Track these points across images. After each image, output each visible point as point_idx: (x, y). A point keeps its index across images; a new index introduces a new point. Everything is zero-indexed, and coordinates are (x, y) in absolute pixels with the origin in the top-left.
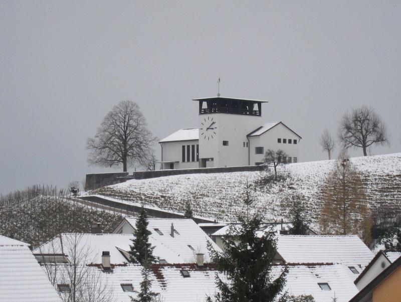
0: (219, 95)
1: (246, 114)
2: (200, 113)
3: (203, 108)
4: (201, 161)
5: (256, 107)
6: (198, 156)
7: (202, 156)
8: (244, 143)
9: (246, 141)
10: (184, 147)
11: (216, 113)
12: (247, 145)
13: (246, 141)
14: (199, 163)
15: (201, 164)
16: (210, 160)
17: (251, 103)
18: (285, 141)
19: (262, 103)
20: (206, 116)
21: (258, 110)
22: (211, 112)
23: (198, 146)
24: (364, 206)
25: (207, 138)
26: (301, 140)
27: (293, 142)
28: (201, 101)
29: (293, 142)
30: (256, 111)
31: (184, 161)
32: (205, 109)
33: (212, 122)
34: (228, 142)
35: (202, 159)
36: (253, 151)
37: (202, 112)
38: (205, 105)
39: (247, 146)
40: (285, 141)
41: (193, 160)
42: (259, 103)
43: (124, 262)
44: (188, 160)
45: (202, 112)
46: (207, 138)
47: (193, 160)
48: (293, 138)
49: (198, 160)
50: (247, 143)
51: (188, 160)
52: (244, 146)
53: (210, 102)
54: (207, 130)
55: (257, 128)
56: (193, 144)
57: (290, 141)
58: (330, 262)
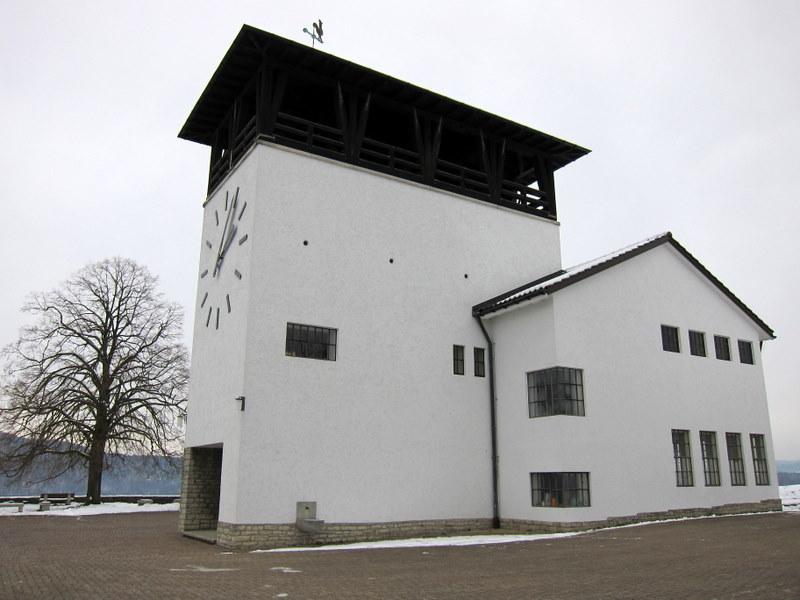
8: (458, 351)
9: (472, 340)
13: (472, 340)
36: (515, 394)
39: (479, 373)
48: (738, 331)
50: (478, 352)
52: (459, 369)
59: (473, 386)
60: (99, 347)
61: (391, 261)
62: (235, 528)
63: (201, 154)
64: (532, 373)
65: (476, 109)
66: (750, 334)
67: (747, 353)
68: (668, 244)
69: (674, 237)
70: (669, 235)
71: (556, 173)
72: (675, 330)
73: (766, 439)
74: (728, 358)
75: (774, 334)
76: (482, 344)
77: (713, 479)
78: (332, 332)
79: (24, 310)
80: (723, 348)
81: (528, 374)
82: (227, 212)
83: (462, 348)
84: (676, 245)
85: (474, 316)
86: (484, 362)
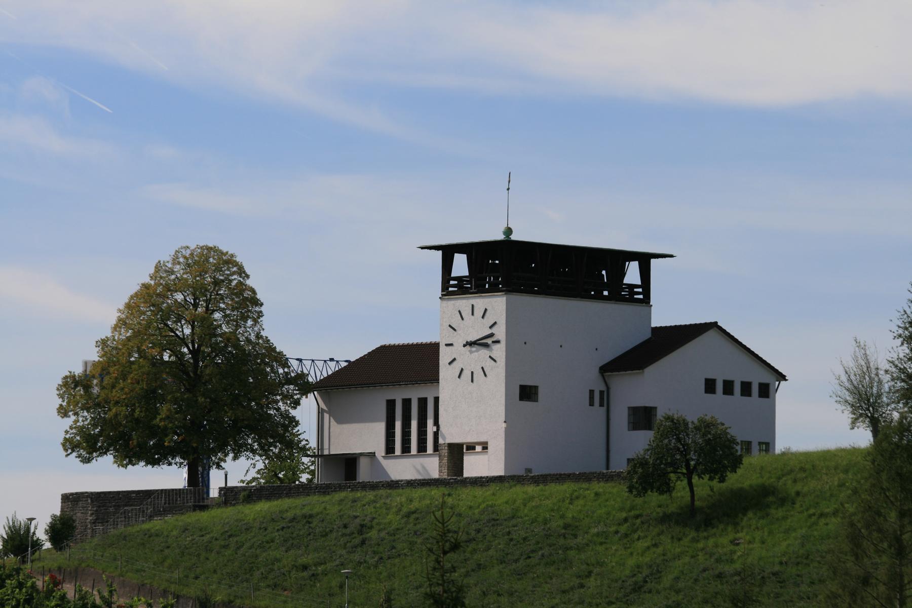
8: (592, 392)
9: (599, 386)
13: (599, 386)
36: (620, 418)
39: (601, 405)
48: (757, 377)
50: (602, 393)
52: (592, 404)
62: (440, 471)
65: (660, 359)
66: (766, 378)
70: (716, 323)
71: (650, 336)
73: (771, 446)
74: (750, 395)
76: (603, 388)
77: (407, 403)
78: (536, 387)
82: (604, 408)
86: (604, 399)
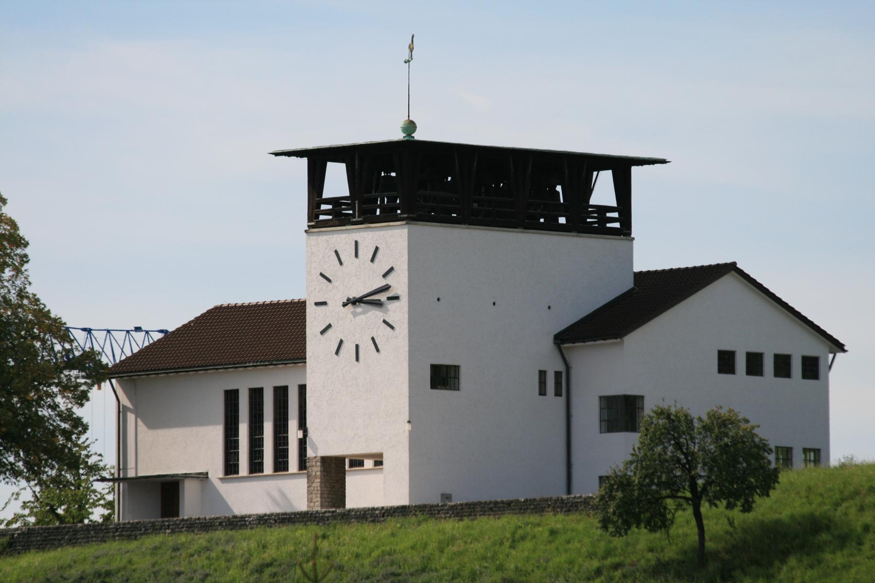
0: (410, 126)
1: (552, 227)
2: (315, 221)
3: (325, 195)
4: (316, 469)
5: (603, 191)
6: (302, 443)
7: (325, 442)
8: (542, 374)
9: (553, 365)
10: (231, 397)
11: (396, 219)
12: (558, 384)
13: (553, 365)
14: (310, 482)
15: (317, 483)
16: (369, 464)
17: (579, 168)
18: (754, 364)
19: (635, 170)
20: (342, 239)
21: (613, 203)
22: (367, 217)
23: (302, 389)
24: (712, 463)
25: (348, 350)
26: (840, 355)
27: (797, 367)
28: (317, 160)
29: (797, 367)
30: (602, 210)
31: (231, 468)
32: (335, 202)
33: (382, 283)
34: (456, 368)
35: (325, 460)
36: (588, 413)
37: (324, 214)
38: (337, 181)
39: (558, 393)
40: (754, 364)
41: (281, 464)
42: (621, 168)
43: (103, 515)
44: (256, 466)
45: (324, 214)
46: (348, 350)
47: (281, 464)
48: (799, 346)
49: (303, 464)
50: (558, 374)
51: (256, 466)
52: (542, 392)
53: (362, 159)
54: (344, 305)
55: (354, 247)
56: (280, 383)
57: (783, 366)
58: (342, 351)
59: (554, 404)
60: (118, 361)
61: (494, 304)
62: (310, 500)
63: (89, 395)
64: (605, 397)
66: (813, 347)
67: (812, 369)
68: (733, 272)
69: (738, 266)
70: (734, 264)
72: (805, 376)
73: (823, 454)
74: (777, 357)
75: (846, 348)
76: (561, 367)
77: (256, 395)
79: (344, 305)
80: (783, 366)
81: (601, 397)
83: (540, 394)
84: (741, 273)
85: (555, 343)
